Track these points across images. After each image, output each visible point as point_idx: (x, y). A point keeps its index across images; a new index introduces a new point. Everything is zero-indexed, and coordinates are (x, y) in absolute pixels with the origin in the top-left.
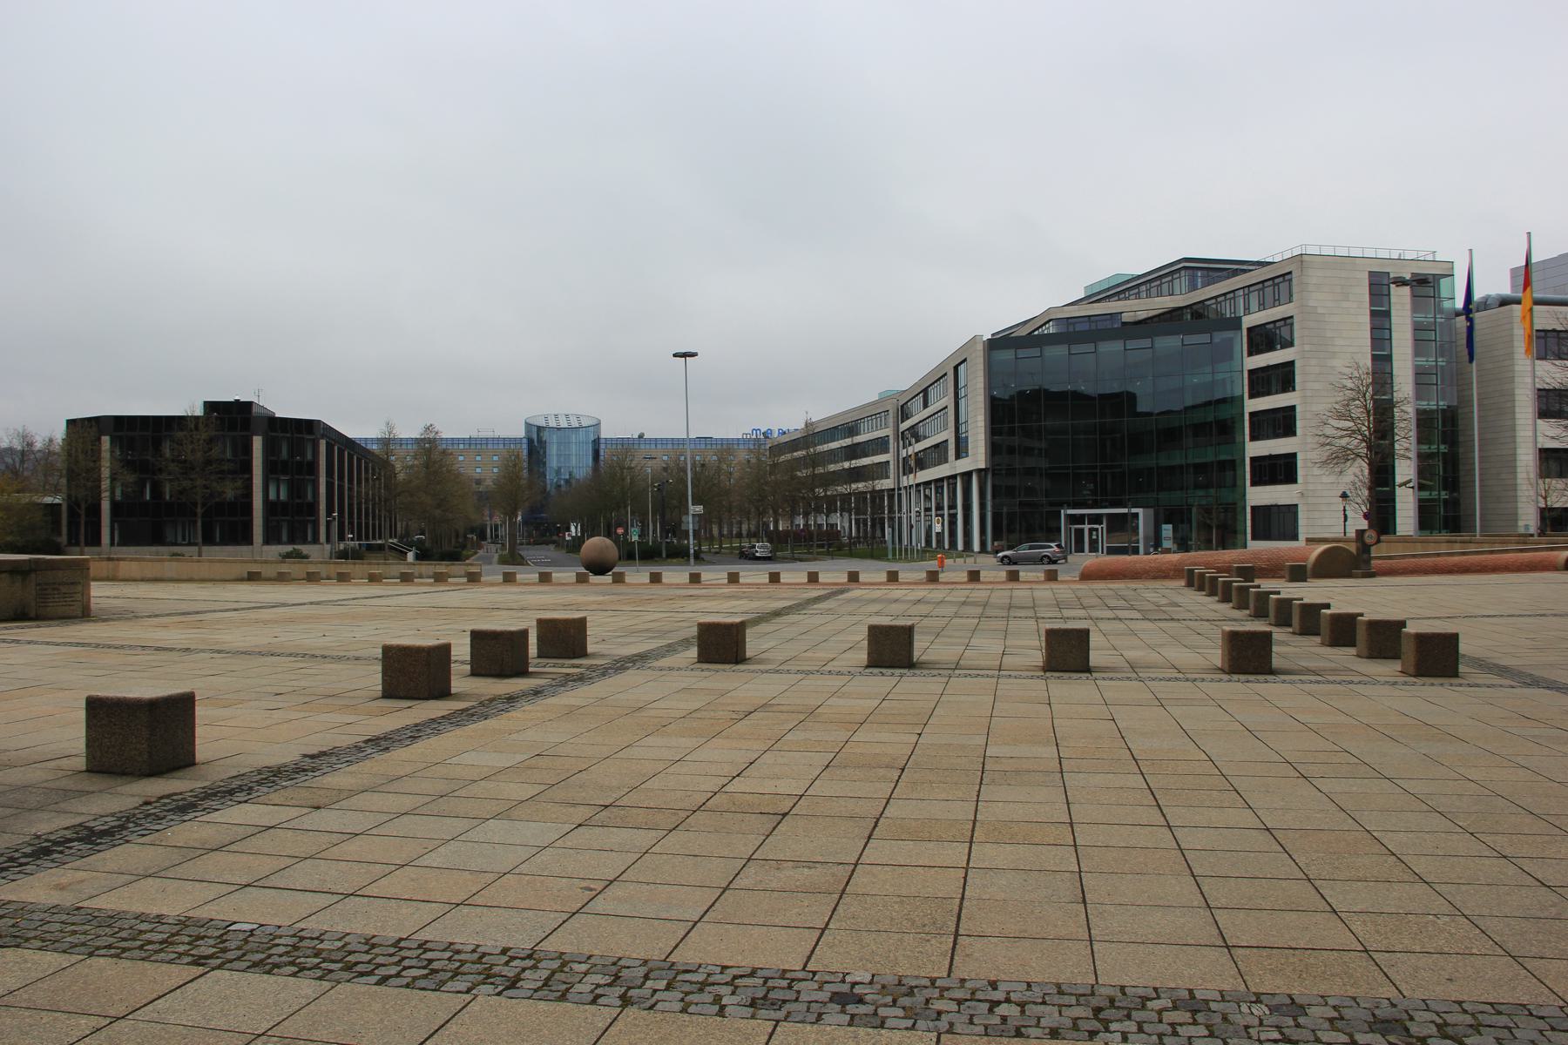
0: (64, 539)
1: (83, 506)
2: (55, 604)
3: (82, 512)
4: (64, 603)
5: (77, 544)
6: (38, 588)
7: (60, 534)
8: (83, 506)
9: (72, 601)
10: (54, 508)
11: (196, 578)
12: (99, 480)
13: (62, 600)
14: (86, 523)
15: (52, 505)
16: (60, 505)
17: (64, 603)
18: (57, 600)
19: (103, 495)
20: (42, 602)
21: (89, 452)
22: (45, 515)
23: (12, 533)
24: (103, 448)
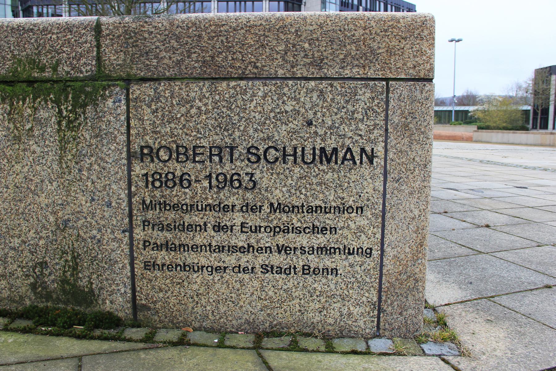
0: (530, 126)
1: (540, 108)
2: (230, 260)
3: (539, 112)
4: (277, 259)
5: (536, 128)
6: (138, 169)
7: (529, 124)
8: (540, 108)
9: (323, 250)
10: (526, 112)
11: (484, 140)
12: (549, 95)
13: (265, 240)
14: (541, 118)
15: (526, 111)
16: (529, 110)
17: (277, 259)
18: (240, 240)
19: (551, 103)
20: (167, 246)
21: (545, 82)
22: (522, 114)
23: (506, 122)
24: (551, 93)
